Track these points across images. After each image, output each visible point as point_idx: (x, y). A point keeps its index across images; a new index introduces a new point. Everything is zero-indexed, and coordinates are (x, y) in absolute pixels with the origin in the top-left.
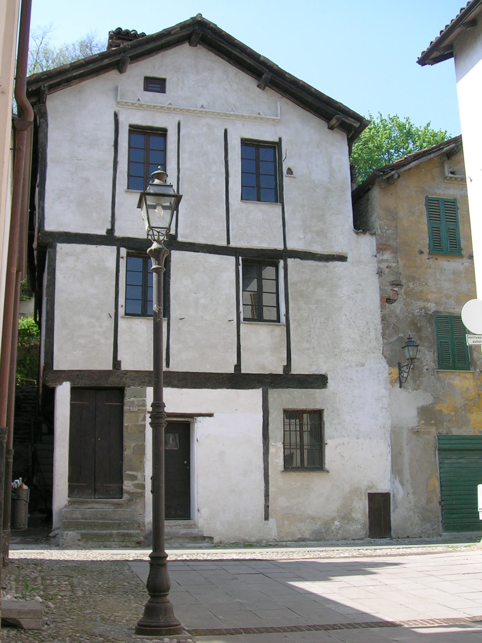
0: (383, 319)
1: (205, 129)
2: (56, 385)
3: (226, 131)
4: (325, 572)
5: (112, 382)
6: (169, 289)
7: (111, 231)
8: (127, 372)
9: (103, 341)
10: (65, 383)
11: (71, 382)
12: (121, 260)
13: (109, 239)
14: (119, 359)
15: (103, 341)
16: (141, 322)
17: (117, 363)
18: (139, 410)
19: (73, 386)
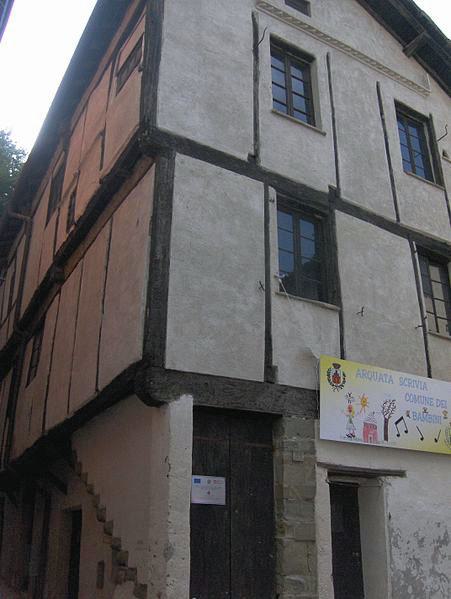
0: (316, 576)
1: (356, 73)
2: (169, 398)
3: (378, 83)
4: (72, 208)
5: (264, 404)
6: (334, 237)
7: (254, 157)
8: (286, 389)
9: (249, 328)
10: (183, 397)
11: (194, 397)
12: (270, 203)
13: (250, 167)
14: (274, 363)
15: (249, 328)
16: (304, 307)
17: (270, 369)
18: (305, 459)
19: (197, 404)
